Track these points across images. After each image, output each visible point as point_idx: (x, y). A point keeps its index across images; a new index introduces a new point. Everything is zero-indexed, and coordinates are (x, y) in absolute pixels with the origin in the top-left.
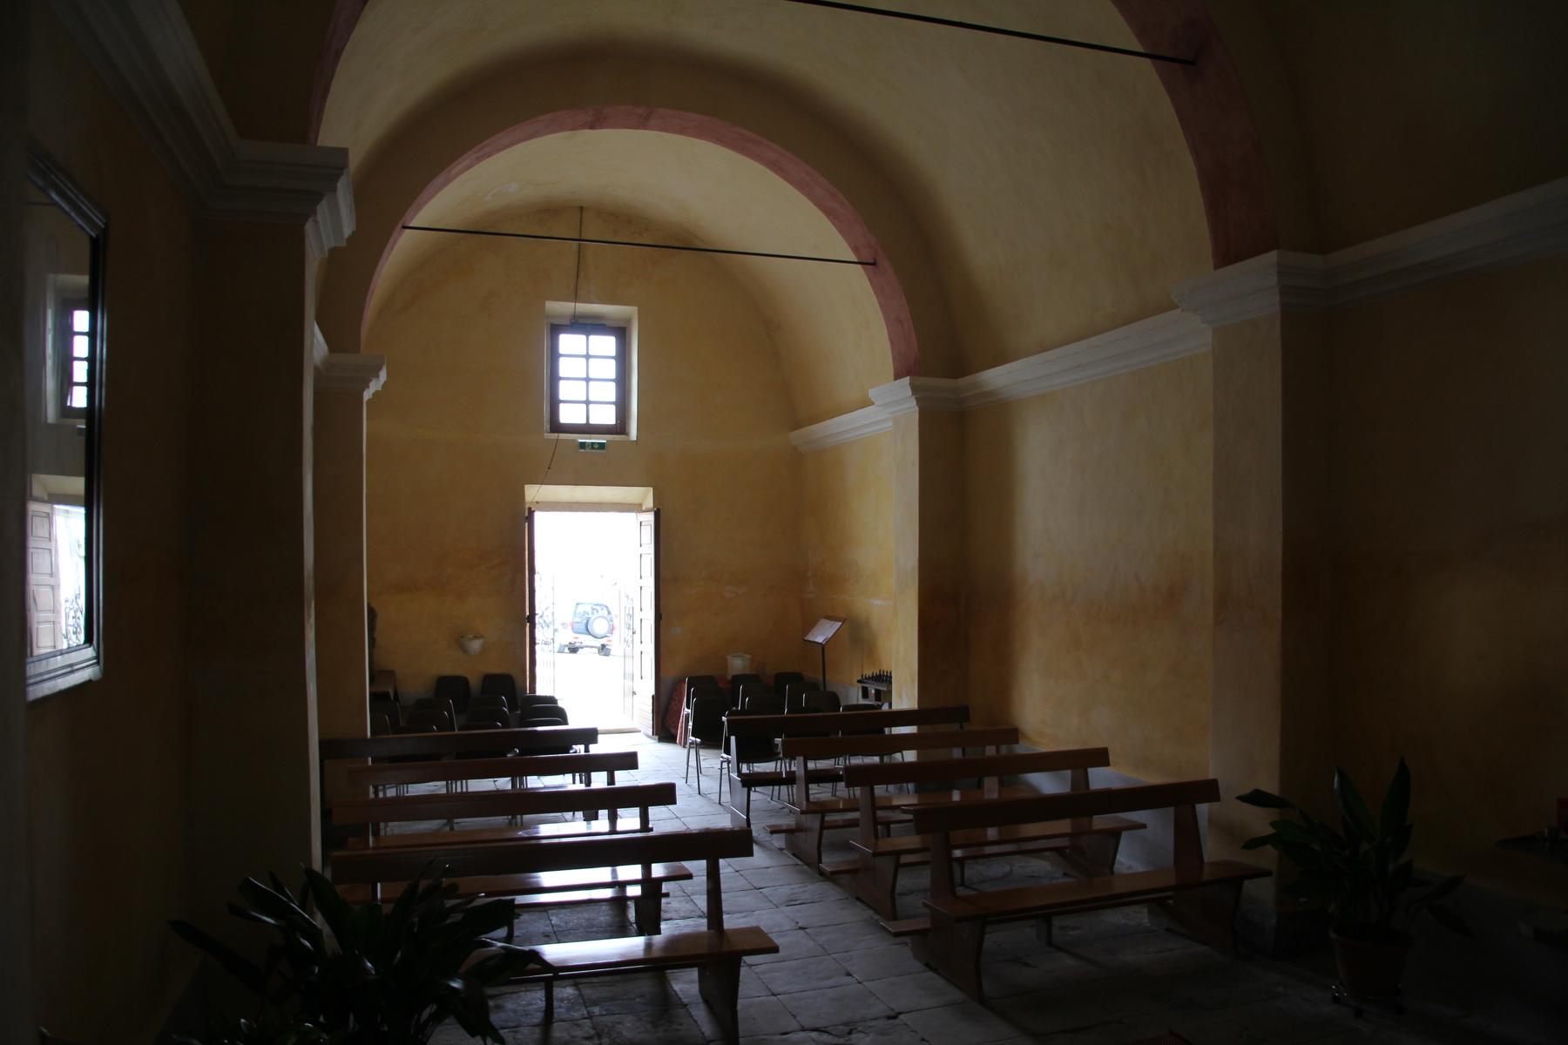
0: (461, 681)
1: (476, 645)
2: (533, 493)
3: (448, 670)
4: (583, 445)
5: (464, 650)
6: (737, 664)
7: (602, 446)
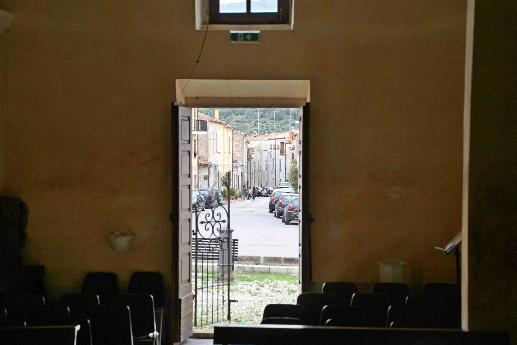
0: (111, 277)
1: (122, 242)
2: (184, 88)
3: (98, 265)
4: (235, 37)
5: (112, 247)
6: (388, 273)
7: (255, 37)
